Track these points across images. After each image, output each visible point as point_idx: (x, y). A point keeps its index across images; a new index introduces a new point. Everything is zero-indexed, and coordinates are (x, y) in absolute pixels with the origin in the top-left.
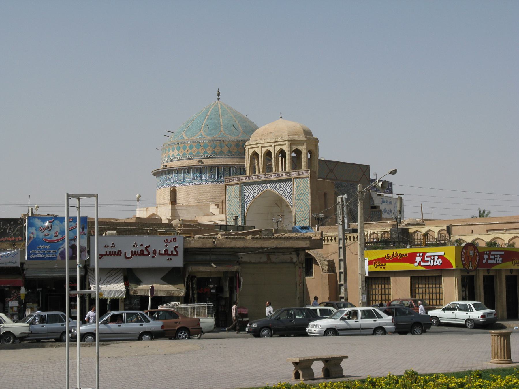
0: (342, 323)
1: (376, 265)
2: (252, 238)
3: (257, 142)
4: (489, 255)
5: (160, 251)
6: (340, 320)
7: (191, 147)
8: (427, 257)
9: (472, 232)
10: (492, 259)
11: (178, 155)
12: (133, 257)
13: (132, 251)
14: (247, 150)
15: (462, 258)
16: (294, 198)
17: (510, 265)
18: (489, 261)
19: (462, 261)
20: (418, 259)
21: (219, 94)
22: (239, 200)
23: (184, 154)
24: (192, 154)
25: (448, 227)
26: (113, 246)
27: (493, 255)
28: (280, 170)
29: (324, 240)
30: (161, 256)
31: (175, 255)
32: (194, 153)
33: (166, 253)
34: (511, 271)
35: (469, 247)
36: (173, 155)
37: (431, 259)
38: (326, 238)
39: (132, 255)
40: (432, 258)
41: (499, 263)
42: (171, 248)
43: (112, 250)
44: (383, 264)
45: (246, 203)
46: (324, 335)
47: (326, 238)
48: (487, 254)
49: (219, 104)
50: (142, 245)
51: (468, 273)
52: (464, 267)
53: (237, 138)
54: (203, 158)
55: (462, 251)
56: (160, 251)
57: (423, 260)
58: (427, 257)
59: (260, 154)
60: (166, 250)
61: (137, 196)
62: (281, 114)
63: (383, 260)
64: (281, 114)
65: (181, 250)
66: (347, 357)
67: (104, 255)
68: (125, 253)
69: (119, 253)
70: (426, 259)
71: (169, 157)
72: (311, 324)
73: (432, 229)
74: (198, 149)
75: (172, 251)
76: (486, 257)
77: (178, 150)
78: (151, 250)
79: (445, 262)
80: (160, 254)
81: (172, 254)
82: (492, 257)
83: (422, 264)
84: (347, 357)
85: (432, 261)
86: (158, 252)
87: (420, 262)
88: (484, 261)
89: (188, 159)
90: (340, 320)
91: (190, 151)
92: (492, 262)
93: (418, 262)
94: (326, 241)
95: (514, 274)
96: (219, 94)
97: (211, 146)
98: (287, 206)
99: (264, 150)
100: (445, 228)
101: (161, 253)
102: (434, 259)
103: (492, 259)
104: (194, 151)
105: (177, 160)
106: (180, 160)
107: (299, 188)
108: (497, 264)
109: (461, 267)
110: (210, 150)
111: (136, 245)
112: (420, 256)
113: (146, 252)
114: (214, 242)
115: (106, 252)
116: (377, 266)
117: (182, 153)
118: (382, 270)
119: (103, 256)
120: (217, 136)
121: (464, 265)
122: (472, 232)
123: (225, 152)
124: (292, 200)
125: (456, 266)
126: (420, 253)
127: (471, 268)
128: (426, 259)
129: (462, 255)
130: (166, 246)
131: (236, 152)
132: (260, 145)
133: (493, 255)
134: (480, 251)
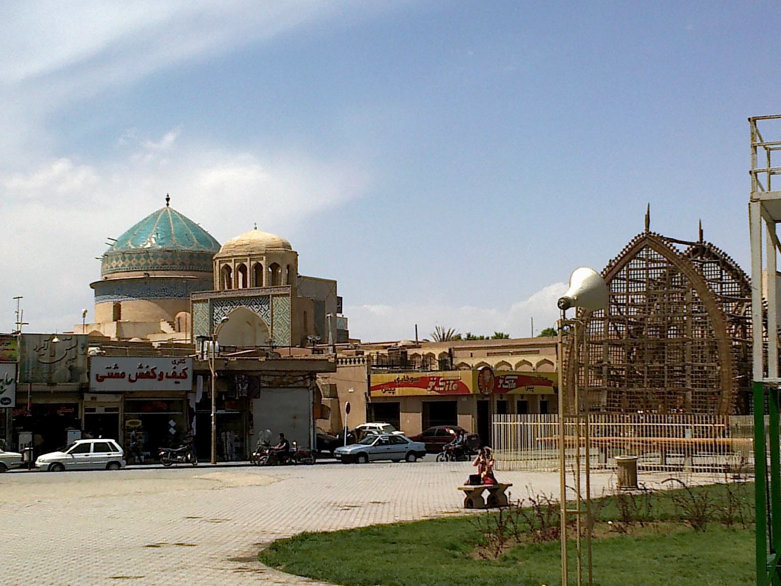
0: (69, 457)
1: (384, 390)
2: (266, 359)
3: (230, 254)
4: (504, 380)
5: (167, 373)
6: (68, 453)
7: (138, 258)
8: (442, 381)
9: (472, 356)
10: (507, 384)
11: (123, 266)
12: (139, 380)
13: (137, 374)
14: (218, 263)
15: (479, 382)
16: (272, 316)
17: (522, 390)
18: (504, 386)
19: (479, 386)
20: (432, 384)
21: (168, 199)
22: (207, 317)
23: (130, 265)
24: (140, 265)
25: (450, 350)
26: (116, 367)
27: (508, 380)
28: (241, 287)
29: (338, 362)
30: (169, 379)
31: (183, 378)
32: (142, 264)
33: (174, 375)
34: (522, 396)
35: (486, 371)
36: (117, 266)
37: (446, 384)
38: (340, 360)
39: (137, 377)
40: (447, 382)
41: (513, 388)
42: (179, 371)
43: (115, 371)
44: (393, 389)
45: (216, 320)
46: (49, 471)
47: (340, 360)
48: (502, 379)
49: (169, 211)
50: (148, 367)
51: (483, 398)
52: (481, 392)
53: (191, 248)
54: (149, 270)
55: (479, 376)
56: (167, 373)
57: (437, 385)
58: (442, 381)
59: (233, 268)
60: (174, 373)
61: (84, 310)
62: (255, 224)
63: (392, 385)
64: (255, 224)
65: (189, 373)
66: (511, 485)
67: (106, 377)
68: (130, 375)
69: (123, 375)
70: (441, 384)
71: (112, 267)
72: (39, 458)
73: (432, 351)
74: (147, 260)
75: (180, 374)
76: (501, 381)
77: (124, 261)
78: (157, 372)
79: (462, 386)
80: (167, 377)
81: (180, 377)
82: (507, 382)
83: (436, 388)
84: (511, 485)
85: (447, 386)
86: (165, 375)
87: (434, 387)
88: (499, 386)
90: (68, 453)
91: (137, 261)
92: (506, 387)
93: (431, 387)
94: (340, 363)
95: (525, 399)
96: (168, 199)
97: (162, 257)
98: (262, 324)
99: (253, 263)
100: (447, 351)
101: (168, 375)
102: (449, 384)
103: (507, 384)
104: (143, 262)
105: (122, 272)
106: (125, 272)
107: (278, 305)
108: (511, 389)
109: (478, 392)
110: (160, 261)
111: (141, 367)
112: (433, 381)
113: (151, 374)
114: (226, 364)
115: (109, 374)
116: (385, 391)
118: (391, 394)
119: (105, 379)
120: (169, 246)
121: (481, 390)
122: (472, 356)
124: (270, 318)
125: (474, 391)
126: (433, 377)
127: (487, 393)
128: (441, 384)
129: (479, 380)
130: (175, 368)
132: (233, 259)
133: (508, 380)
134: (496, 375)
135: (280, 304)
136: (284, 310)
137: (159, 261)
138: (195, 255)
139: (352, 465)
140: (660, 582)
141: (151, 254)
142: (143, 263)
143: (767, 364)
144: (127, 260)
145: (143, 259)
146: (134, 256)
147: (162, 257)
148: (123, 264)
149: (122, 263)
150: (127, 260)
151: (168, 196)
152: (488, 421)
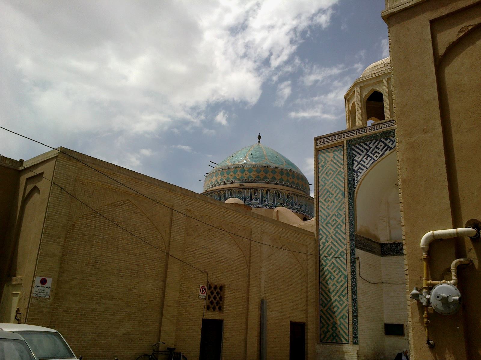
7: (235, 173)
21: (259, 138)
24: (236, 178)
36: (217, 181)
89: (231, 183)
96: (259, 138)
97: (256, 171)
104: (238, 176)
117: (226, 178)
123: (270, 177)
131: (272, 178)
135: (330, 241)
136: (336, 252)
137: (253, 175)
138: (285, 172)
139: (18, 257)
140: (59, 226)
141: (246, 169)
142: (240, 176)
143: (278, 215)
144: (225, 174)
145: (239, 173)
146: (232, 170)
147: (256, 171)
148: (222, 178)
149: (220, 177)
150: (225, 174)
151: (259, 135)
152: (221, 342)
